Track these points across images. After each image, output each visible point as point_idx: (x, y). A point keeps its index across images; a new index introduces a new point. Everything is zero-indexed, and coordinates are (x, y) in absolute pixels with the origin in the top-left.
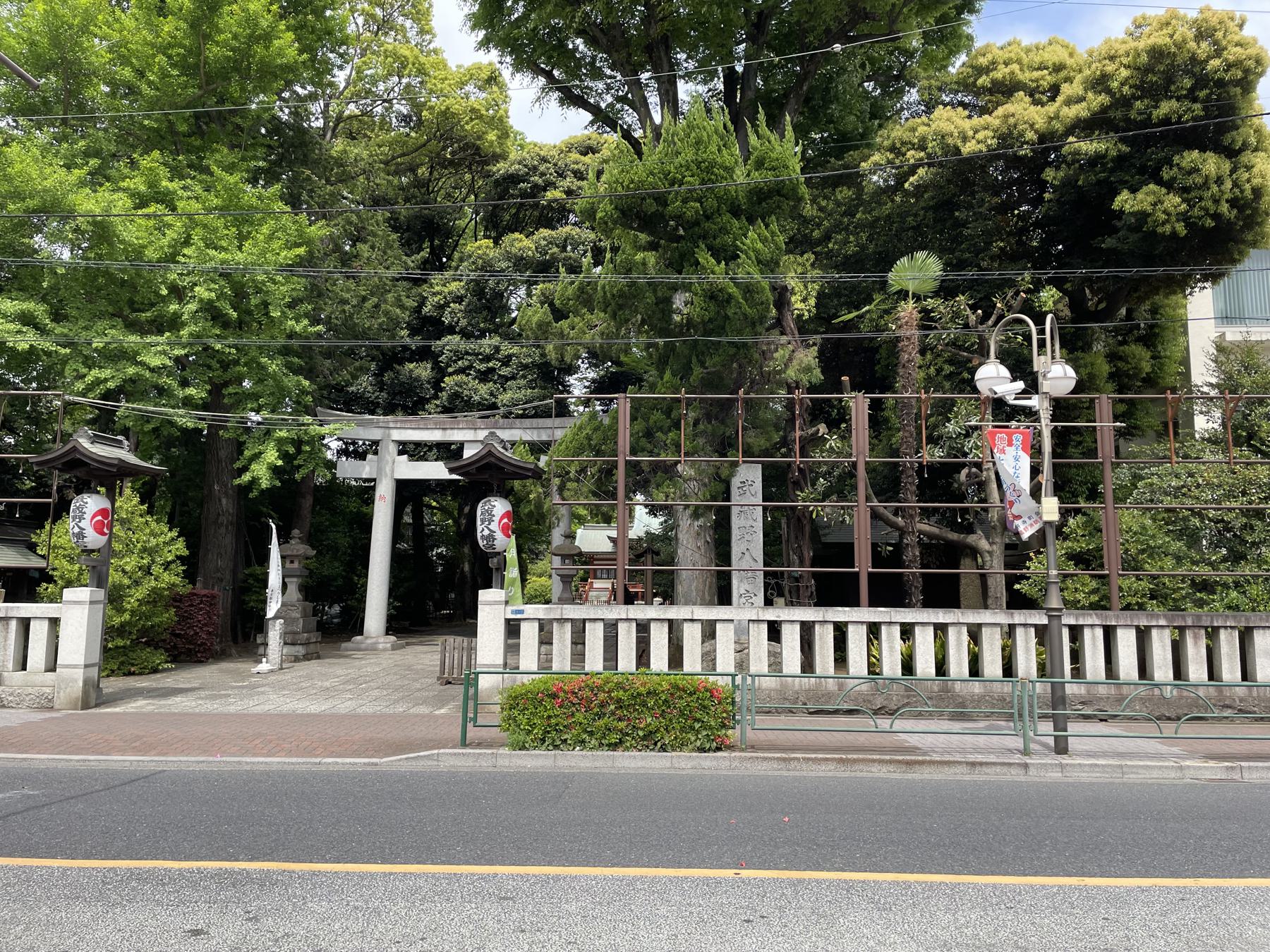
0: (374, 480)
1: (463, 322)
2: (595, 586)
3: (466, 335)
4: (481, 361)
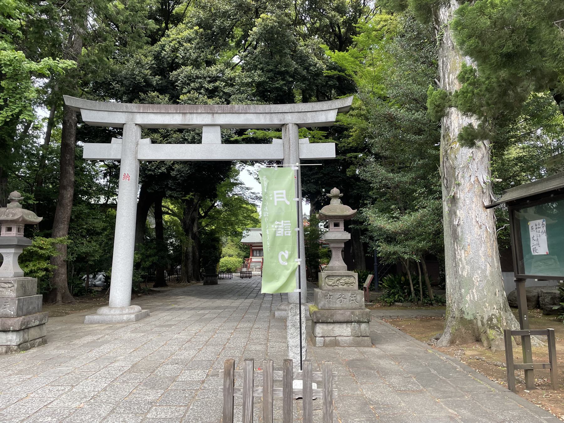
0: (119, 161)
1: (194, 56)
2: (253, 260)
3: (196, 64)
4: (209, 82)
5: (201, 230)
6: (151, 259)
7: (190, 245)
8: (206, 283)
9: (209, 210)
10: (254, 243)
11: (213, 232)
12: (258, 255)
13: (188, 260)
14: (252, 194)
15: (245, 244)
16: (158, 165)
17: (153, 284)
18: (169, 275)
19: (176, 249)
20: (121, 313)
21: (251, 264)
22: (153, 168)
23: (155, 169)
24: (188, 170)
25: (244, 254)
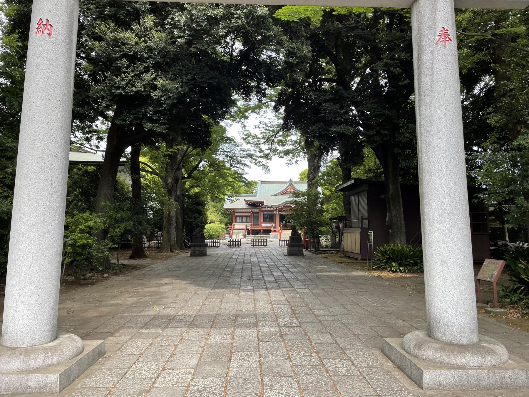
2: (236, 227)
5: (184, 194)
6: (123, 225)
7: (173, 207)
8: (193, 255)
9: (192, 172)
10: (237, 209)
11: (197, 195)
12: (241, 221)
13: (171, 225)
14: (242, 152)
15: (227, 210)
16: (130, 80)
17: (130, 253)
18: (149, 241)
19: (156, 212)
20: (23, 366)
21: (234, 231)
22: (123, 83)
23: (127, 85)
24: (178, 88)
25: (226, 220)
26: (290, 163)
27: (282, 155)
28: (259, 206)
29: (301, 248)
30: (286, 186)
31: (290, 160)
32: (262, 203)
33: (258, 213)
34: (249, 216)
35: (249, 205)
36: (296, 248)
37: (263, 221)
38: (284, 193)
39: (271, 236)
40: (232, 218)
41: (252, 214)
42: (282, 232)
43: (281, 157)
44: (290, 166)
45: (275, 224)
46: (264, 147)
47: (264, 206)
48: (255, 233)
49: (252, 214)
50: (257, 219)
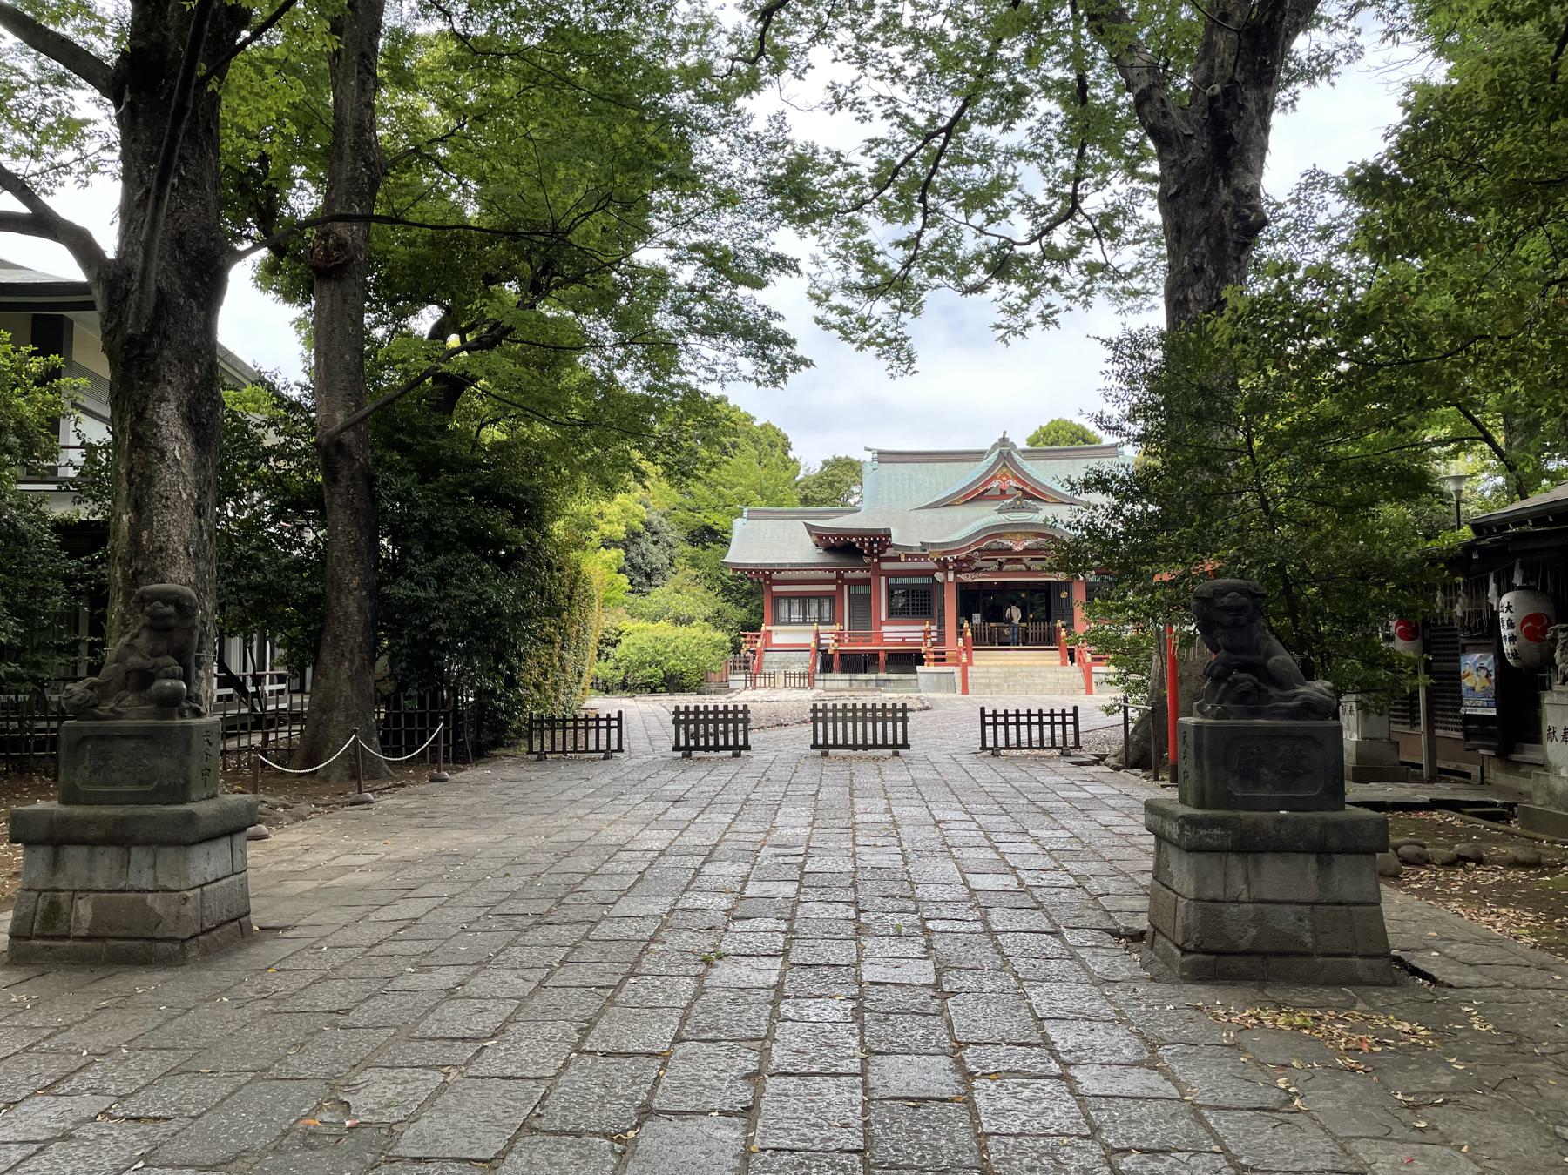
2: (776, 639)
10: (780, 568)
12: (797, 617)
21: (768, 657)
26: (1017, 322)
27: (979, 275)
28: (871, 554)
29: (1346, 879)
30: (982, 467)
31: (1014, 311)
32: (881, 540)
33: (866, 582)
34: (830, 597)
35: (830, 549)
36: (1285, 878)
37: (892, 613)
38: (976, 496)
39: (921, 677)
40: (760, 606)
41: (840, 588)
42: (970, 662)
43: (979, 288)
44: (1015, 340)
45: (941, 625)
46: (881, 233)
47: (889, 552)
48: (855, 663)
49: (840, 588)
50: (862, 608)
